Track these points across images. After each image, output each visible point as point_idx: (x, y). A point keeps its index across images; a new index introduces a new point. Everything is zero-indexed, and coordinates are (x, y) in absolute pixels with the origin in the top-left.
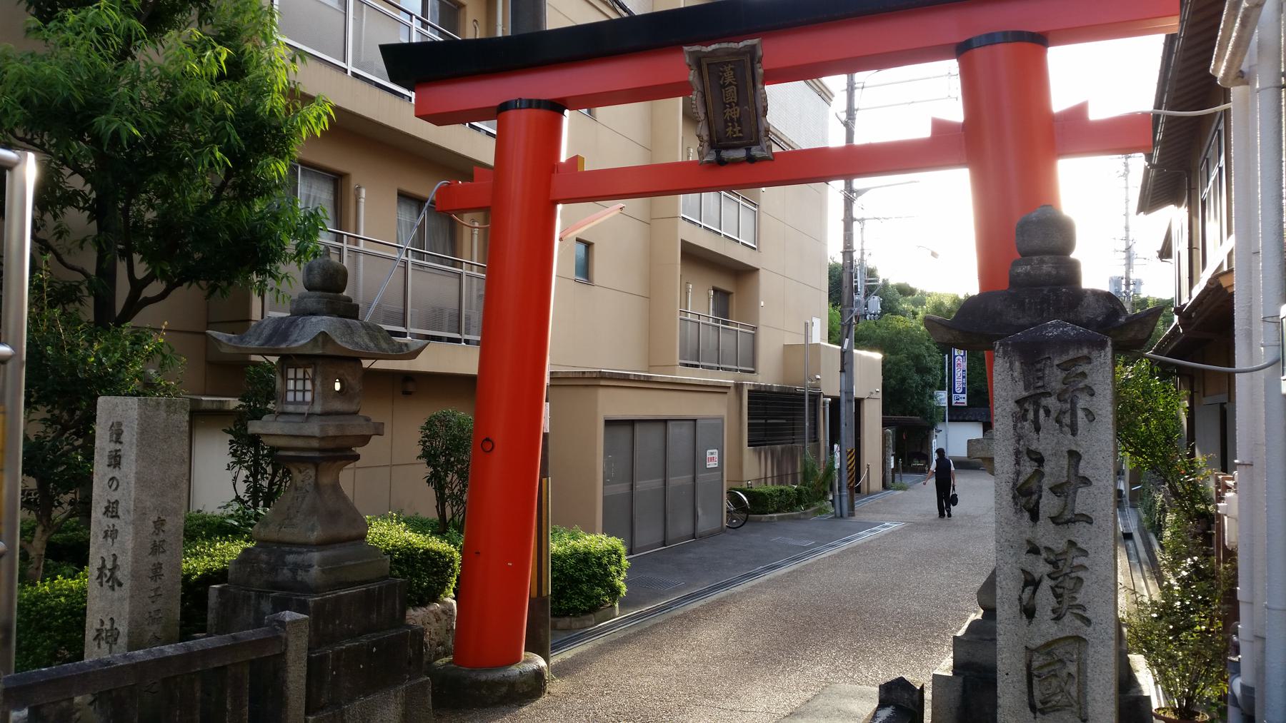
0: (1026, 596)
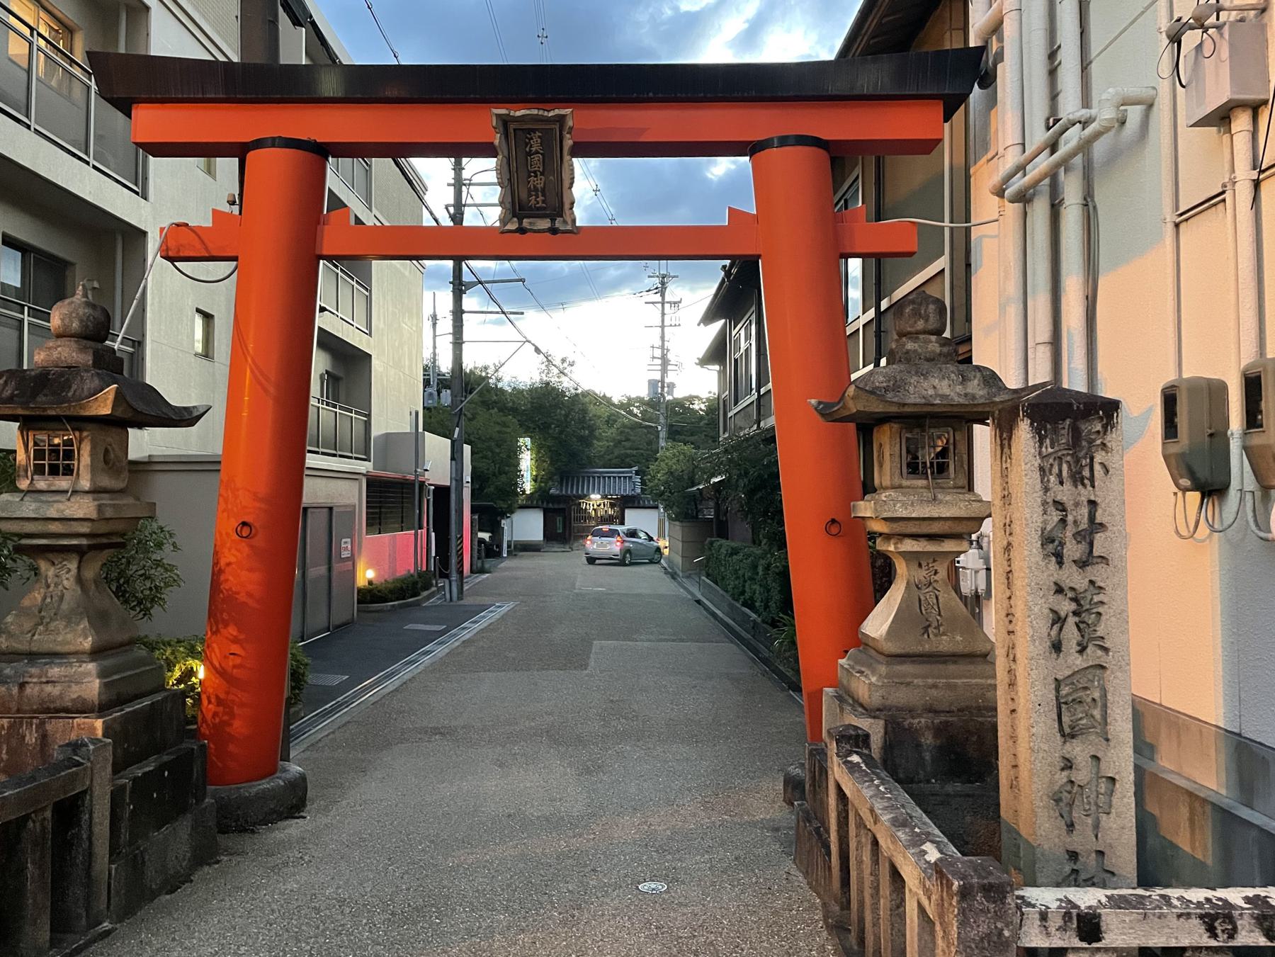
0: (1054, 633)
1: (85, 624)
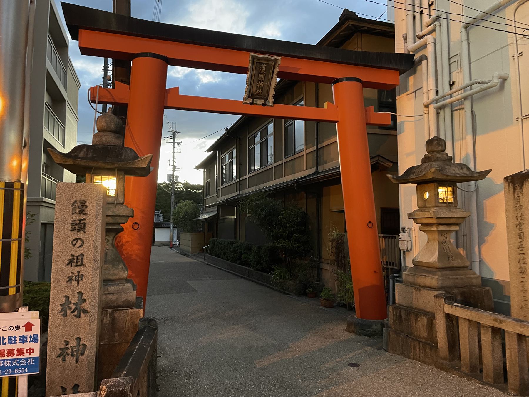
1: (121, 266)
